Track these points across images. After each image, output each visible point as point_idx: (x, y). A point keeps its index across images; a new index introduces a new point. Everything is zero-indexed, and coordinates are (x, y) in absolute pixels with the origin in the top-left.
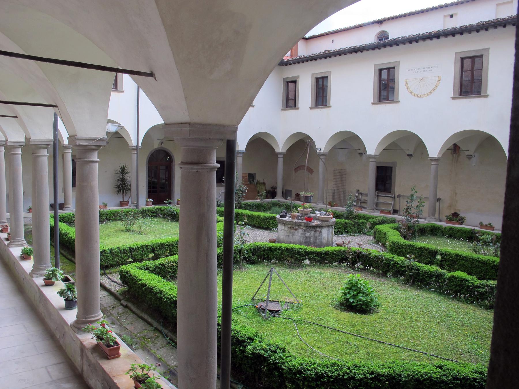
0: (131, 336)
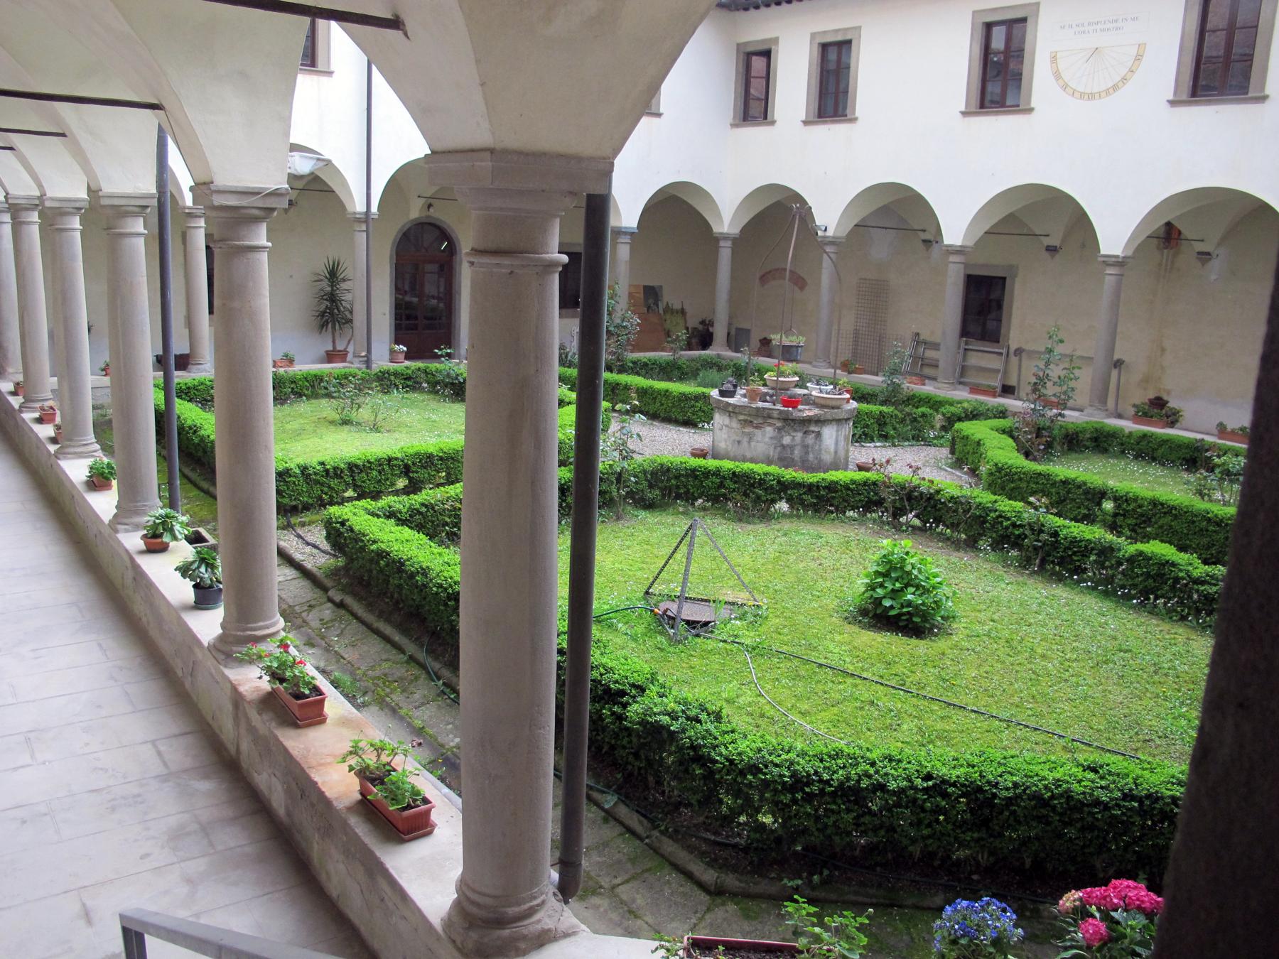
0: (352, 674)
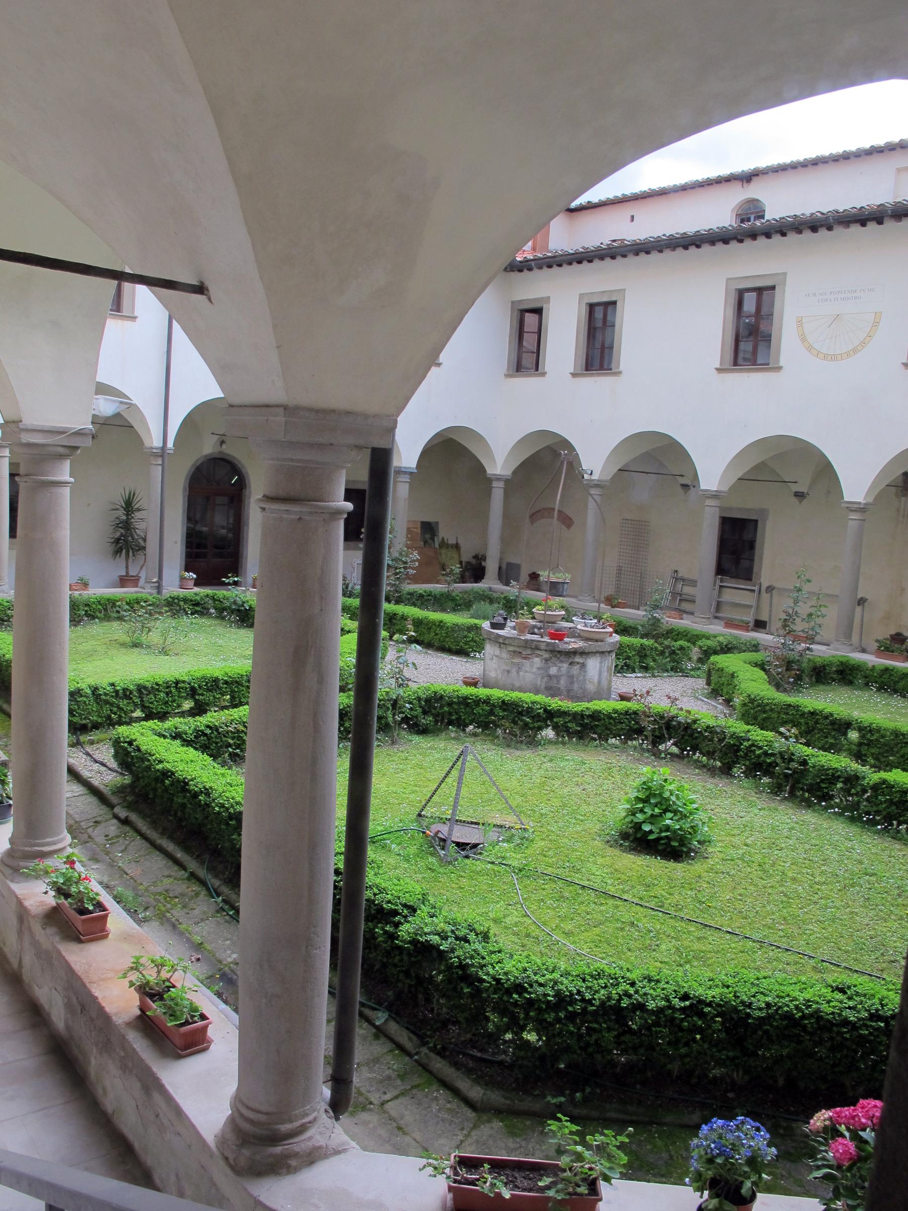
0: (135, 889)
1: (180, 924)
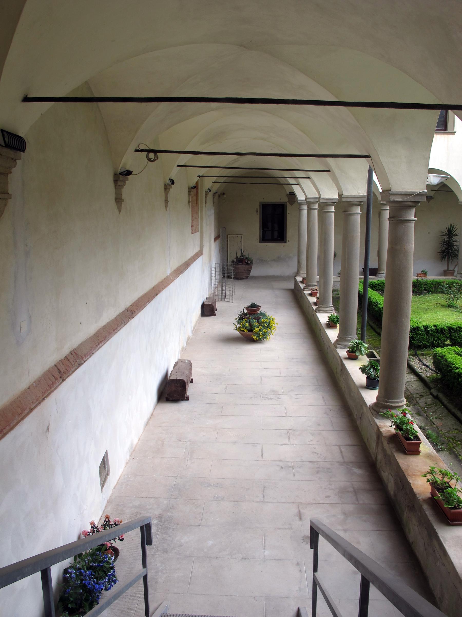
0: (437, 433)
1: (460, 455)
